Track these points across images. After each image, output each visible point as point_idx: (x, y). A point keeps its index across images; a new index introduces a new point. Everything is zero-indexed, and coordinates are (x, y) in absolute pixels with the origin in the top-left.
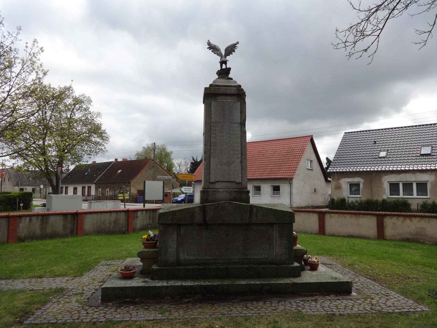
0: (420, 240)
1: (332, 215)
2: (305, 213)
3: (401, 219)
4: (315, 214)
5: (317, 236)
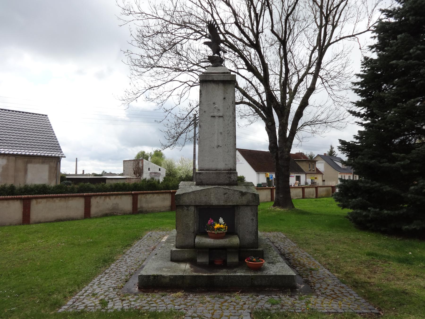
0: (115, 213)
1: (39, 200)
2: (2, 201)
3: (103, 198)
4: (17, 201)
5: (19, 227)
